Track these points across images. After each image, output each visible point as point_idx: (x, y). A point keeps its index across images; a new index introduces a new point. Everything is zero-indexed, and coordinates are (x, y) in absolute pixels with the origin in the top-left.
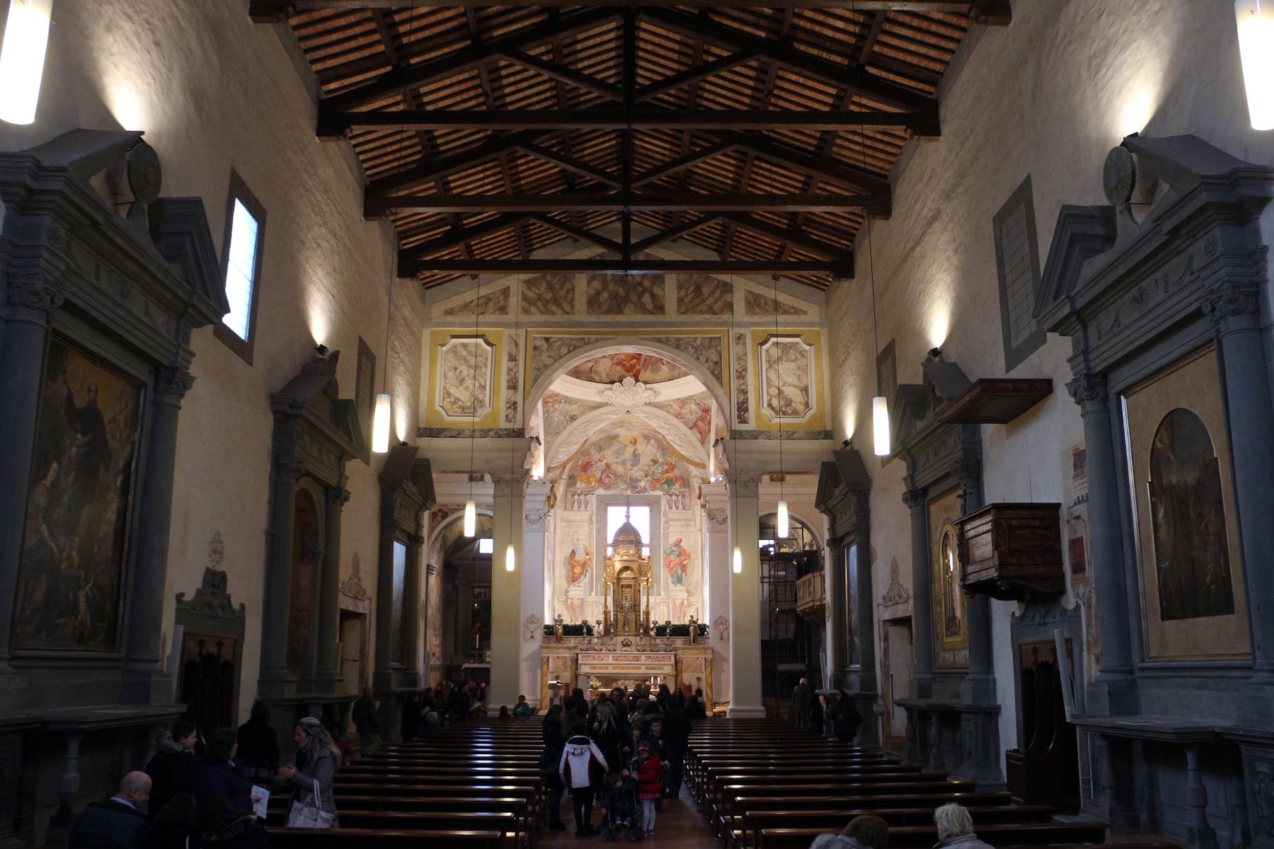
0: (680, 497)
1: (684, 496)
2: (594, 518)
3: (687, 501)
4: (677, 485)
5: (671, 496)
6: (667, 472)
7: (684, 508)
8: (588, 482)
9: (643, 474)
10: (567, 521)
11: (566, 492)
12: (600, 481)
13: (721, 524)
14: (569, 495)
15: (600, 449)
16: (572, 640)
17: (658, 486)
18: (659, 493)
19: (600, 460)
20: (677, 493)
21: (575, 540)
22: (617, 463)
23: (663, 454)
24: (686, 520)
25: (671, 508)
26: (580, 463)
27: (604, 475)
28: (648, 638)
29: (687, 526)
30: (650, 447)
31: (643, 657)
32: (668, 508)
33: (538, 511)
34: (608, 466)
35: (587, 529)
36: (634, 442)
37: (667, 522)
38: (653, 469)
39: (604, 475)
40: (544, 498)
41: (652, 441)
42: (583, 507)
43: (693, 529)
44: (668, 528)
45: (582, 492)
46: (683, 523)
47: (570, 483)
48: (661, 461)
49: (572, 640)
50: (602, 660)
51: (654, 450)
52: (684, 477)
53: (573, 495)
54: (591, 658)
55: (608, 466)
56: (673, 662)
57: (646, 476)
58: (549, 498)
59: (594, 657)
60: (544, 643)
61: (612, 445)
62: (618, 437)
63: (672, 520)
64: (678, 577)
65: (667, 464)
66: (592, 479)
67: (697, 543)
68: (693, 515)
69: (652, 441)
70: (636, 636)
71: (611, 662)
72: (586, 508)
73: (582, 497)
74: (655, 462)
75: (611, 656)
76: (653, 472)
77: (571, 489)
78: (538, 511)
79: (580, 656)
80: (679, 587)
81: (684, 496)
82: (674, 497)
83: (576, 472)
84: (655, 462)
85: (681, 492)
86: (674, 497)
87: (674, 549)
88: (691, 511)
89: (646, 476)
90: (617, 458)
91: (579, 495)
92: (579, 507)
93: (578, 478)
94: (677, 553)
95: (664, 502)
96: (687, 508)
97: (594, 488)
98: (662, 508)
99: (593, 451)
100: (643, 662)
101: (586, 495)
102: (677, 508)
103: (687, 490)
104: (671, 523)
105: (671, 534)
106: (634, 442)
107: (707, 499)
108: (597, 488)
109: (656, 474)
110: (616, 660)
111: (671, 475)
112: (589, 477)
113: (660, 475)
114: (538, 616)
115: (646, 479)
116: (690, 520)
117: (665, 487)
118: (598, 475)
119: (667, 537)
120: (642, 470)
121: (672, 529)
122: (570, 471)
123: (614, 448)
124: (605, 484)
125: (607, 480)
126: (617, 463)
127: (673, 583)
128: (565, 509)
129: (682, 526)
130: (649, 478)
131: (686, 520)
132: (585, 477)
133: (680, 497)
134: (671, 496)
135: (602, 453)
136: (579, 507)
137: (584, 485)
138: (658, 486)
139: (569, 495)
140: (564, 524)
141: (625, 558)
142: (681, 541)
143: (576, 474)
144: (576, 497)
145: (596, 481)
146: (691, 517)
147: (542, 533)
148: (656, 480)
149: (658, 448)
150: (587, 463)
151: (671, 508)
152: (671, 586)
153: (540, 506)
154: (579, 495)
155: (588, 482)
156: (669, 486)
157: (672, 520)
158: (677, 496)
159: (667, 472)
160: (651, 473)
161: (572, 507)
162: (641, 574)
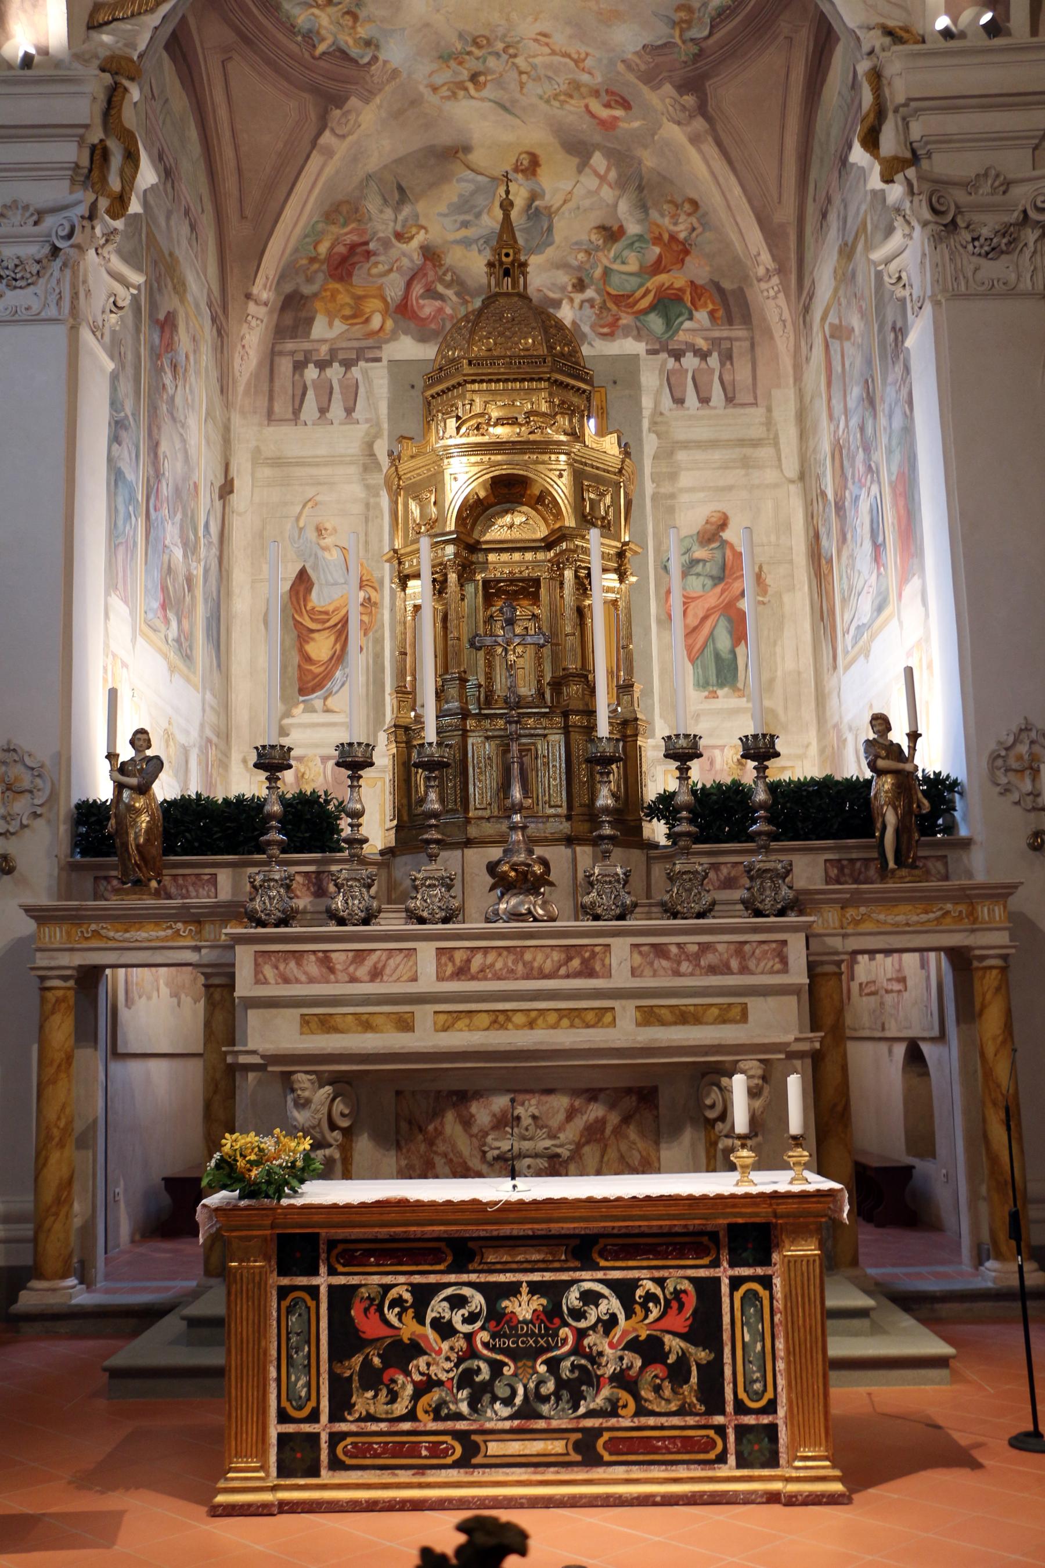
0: (714, 361)
1: (727, 357)
2: (381, 449)
3: (742, 373)
4: (702, 316)
5: (678, 355)
6: (657, 267)
7: (730, 400)
8: (357, 315)
9: (565, 279)
10: (278, 462)
11: (272, 356)
12: (403, 310)
13: (993, 252)
14: (285, 365)
15: (402, 195)
16: (224, 877)
17: (626, 320)
18: (630, 346)
19: (399, 236)
20: (702, 344)
21: (311, 534)
22: (466, 243)
23: (643, 207)
24: (741, 443)
25: (679, 401)
26: (323, 249)
27: (418, 289)
28: (637, 855)
29: (746, 464)
30: (589, 182)
31: (620, 947)
32: (667, 402)
33: (40, 215)
34: (430, 254)
35: (357, 490)
36: (531, 165)
37: (666, 453)
38: (605, 258)
39: (418, 289)
40: (68, 152)
41: (598, 161)
42: (337, 410)
43: (770, 476)
44: (673, 476)
45: (333, 353)
46: (736, 453)
47: (288, 320)
48: (633, 228)
49: (224, 877)
50: (376, 974)
51: (607, 193)
52: (727, 285)
53: (299, 367)
54: (312, 967)
55: (430, 254)
56: (798, 975)
57: (580, 286)
58: (100, 155)
59: (325, 960)
60: (67, 891)
61: (445, 178)
62: (467, 149)
63: (686, 445)
64: (717, 656)
65: (658, 240)
66: (373, 304)
67: (789, 527)
68: (769, 423)
69: (598, 161)
70: (570, 841)
71: (428, 981)
72: (349, 411)
73: (335, 372)
74: (612, 234)
75: (426, 952)
76: (607, 272)
77: (290, 346)
78: (40, 215)
79: (244, 958)
80: (726, 699)
81: (727, 357)
82: (690, 361)
83: (309, 280)
84: (612, 234)
85: (716, 342)
86: (690, 361)
87: (699, 553)
88: (757, 414)
89: (580, 286)
90: (465, 224)
91: (322, 365)
92: (323, 411)
93: (318, 305)
94: (712, 568)
95: (650, 379)
96: (742, 397)
97: (379, 339)
98: (647, 402)
99: (372, 205)
100: (621, 978)
101: (348, 364)
102: (704, 400)
103: (739, 332)
104: (681, 456)
105: (684, 498)
106: (531, 165)
107: (916, 131)
108: (393, 337)
109: (615, 279)
110: (462, 972)
111: (676, 279)
112: (359, 299)
113: (634, 281)
114: (41, 752)
115: (578, 298)
116: (756, 443)
117: (656, 322)
118: (394, 287)
119: (671, 510)
120: (565, 266)
121: (685, 480)
122: (283, 277)
123: (453, 191)
124: (421, 322)
125: (428, 308)
126: (466, 243)
127: (703, 684)
128: (270, 416)
129: (726, 467)
130: (590, 293)
131: (741, 443)
132: (344, 298)
133: (714, 361)
134: (678, 355)
135: (406, 211)
136: (323, 411)
137: (339, 327)
138: (626, 320)
139: (285, 365)
140: (267, 472)
141: (502, 432)
142: (723, 525)
143: (307, 290)
144: (311, 373)
145: (385, 313)
146: (757, 432)
147: (60, 331)
148: (618, 299)
149: (622, 184)
150: (353, 248)
151: (679, 401)
152: (695, 698)
153: (57, 191)
154: (322, 365)
155: (357, 315)
156: (668, 324)
157: (686, 445)
158: (704, 355)
159: (657, 267)
160: (598, 272)
161: (297, 412)
162: (586, 520)
